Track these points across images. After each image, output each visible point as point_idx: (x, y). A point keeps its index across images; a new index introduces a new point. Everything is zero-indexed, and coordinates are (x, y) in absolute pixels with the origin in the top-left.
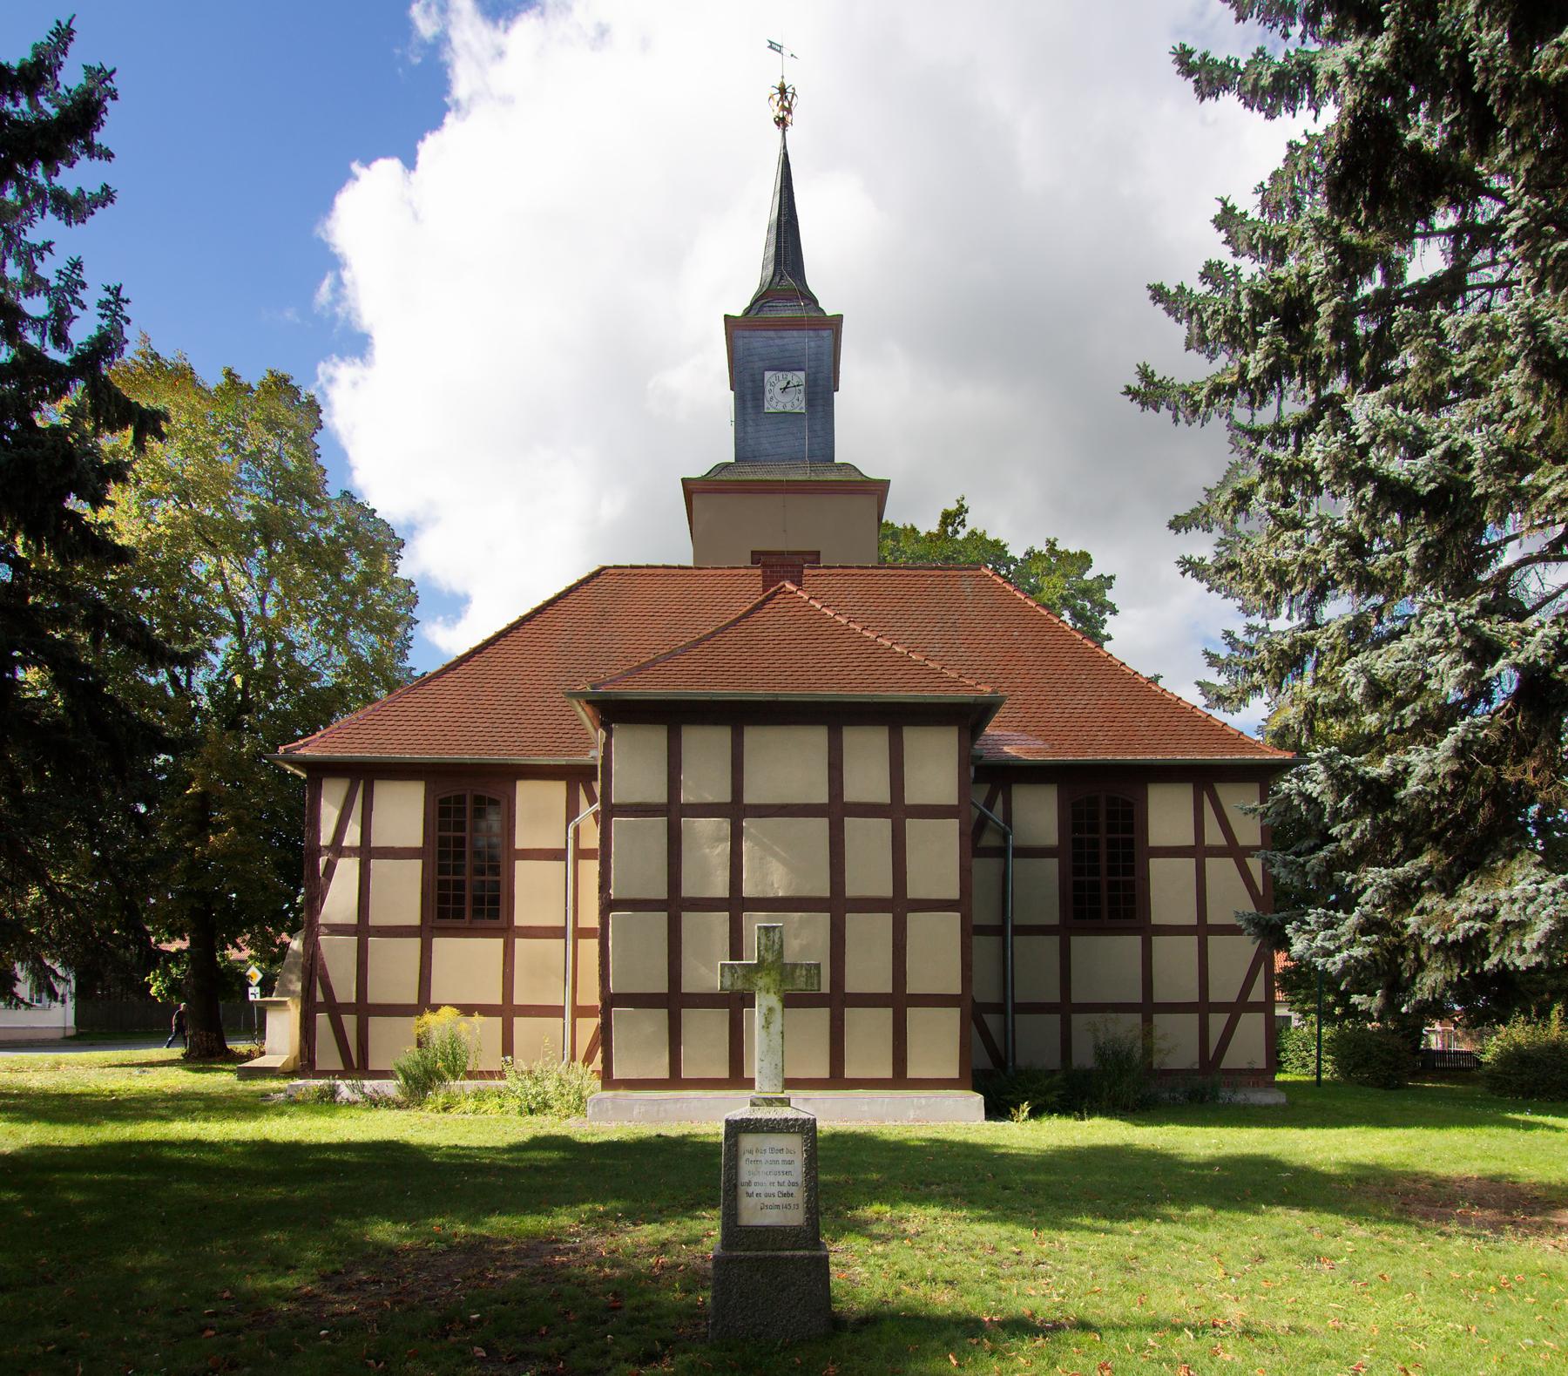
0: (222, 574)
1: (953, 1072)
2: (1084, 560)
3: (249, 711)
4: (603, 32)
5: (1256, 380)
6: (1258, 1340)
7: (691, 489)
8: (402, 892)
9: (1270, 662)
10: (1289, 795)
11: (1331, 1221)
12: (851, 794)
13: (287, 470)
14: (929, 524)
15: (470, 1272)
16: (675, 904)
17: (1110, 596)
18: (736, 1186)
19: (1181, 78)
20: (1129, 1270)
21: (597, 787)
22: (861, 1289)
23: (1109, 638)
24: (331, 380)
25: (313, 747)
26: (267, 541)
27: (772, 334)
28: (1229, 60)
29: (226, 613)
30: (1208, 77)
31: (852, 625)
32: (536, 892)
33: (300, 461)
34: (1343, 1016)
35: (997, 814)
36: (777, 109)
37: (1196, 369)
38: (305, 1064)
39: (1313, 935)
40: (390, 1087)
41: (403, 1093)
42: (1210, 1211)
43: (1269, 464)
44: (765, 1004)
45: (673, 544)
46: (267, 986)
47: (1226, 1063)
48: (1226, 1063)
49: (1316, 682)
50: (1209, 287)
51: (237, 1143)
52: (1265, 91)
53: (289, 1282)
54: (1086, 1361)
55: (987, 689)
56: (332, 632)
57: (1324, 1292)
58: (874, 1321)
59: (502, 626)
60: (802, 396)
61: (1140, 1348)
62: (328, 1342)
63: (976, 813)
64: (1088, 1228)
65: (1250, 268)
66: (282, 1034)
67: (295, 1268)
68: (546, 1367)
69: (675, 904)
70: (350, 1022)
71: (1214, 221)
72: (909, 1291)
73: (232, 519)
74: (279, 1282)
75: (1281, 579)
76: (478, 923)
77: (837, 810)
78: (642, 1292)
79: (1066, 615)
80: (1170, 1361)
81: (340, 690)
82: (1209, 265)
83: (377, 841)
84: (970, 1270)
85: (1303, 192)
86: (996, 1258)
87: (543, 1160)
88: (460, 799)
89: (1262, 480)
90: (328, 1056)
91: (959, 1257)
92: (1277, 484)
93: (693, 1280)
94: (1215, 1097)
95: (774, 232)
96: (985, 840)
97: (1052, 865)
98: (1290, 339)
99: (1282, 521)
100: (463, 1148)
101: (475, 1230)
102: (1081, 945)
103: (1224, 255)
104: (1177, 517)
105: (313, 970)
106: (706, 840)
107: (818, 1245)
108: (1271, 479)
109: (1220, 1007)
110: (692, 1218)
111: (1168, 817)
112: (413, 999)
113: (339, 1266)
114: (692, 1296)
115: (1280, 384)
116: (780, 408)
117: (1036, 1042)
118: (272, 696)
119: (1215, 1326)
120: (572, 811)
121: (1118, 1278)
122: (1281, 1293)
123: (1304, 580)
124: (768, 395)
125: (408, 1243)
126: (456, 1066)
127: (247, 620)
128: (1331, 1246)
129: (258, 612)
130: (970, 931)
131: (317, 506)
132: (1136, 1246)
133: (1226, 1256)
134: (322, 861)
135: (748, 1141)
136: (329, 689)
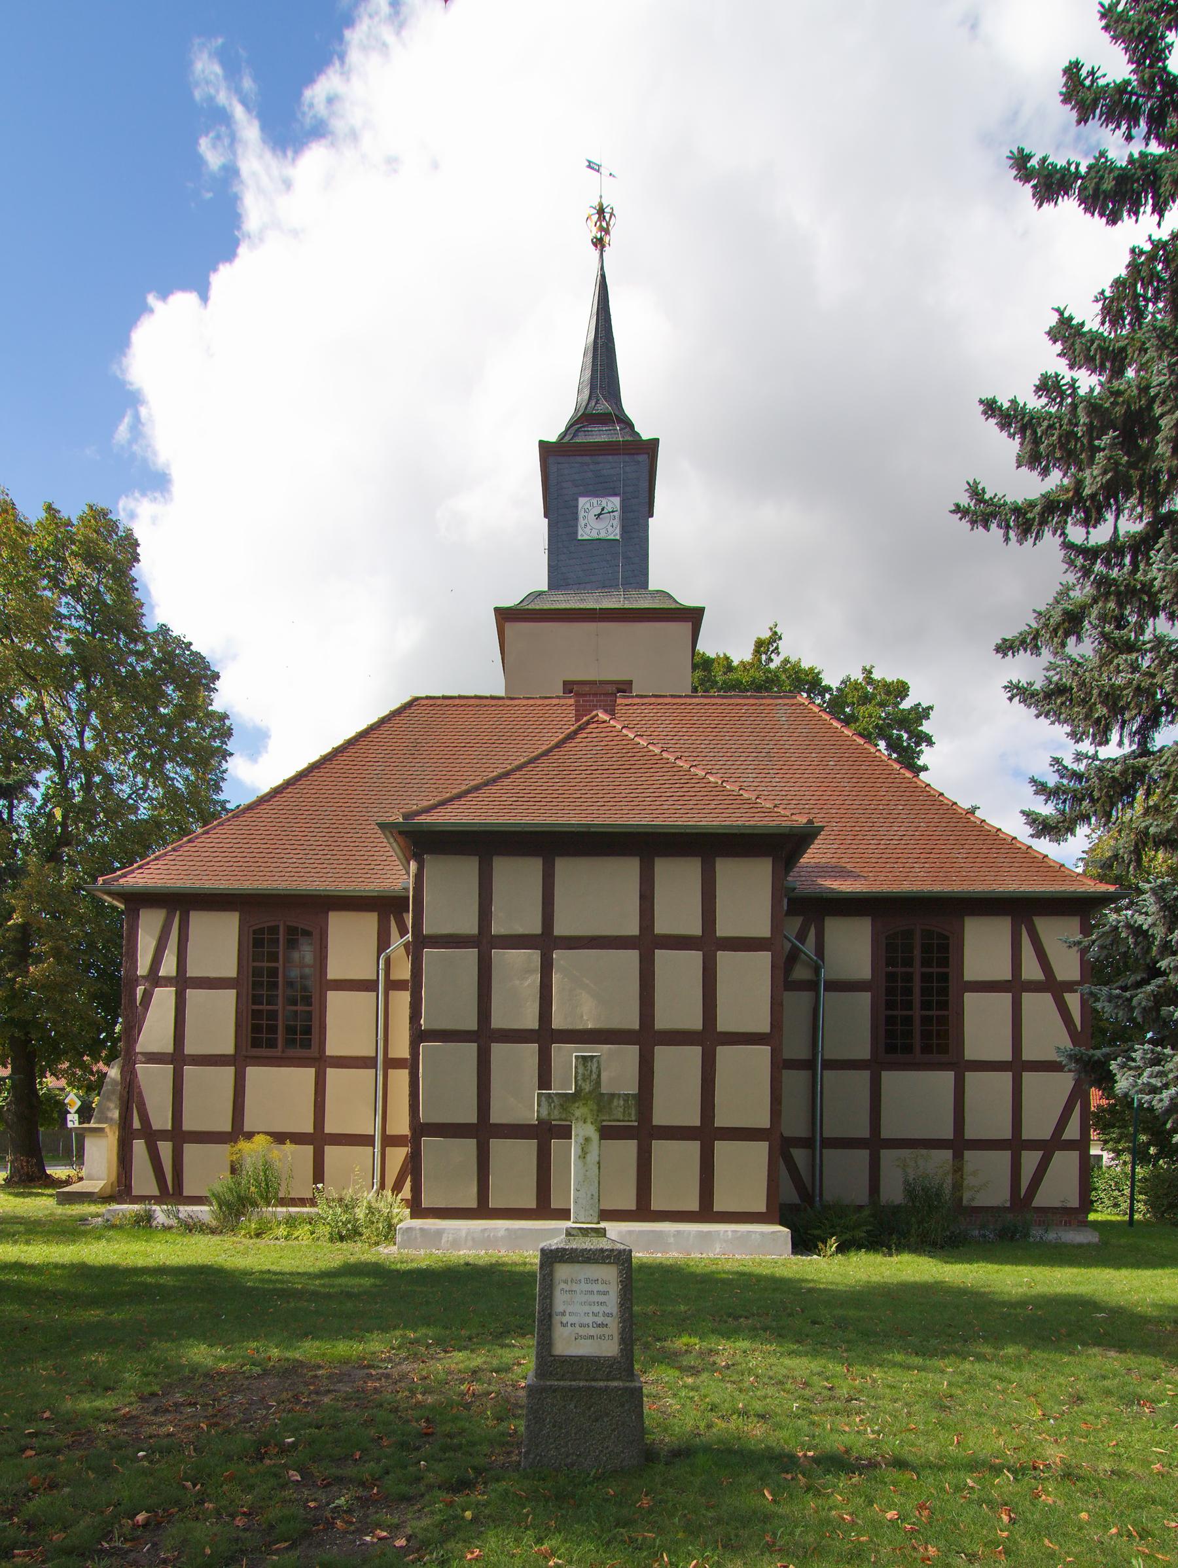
0: (43, 708)
1: (760, 1205)
2: (901, 690)
3: (68, 844)
4: (392, 162)
5: (1093, 497)
6: (1080, 1484)
7: (504, 616)
8: (216, 1020)
9: (1100, 790)
10: (1116, 928)
11: (1151, 1363)
12: (662, 926)
13: (105, 604)
14: (741, 654)
15: (284, 1396)
16: (484, 1036)
17: (926, 727)
18: (550, 1316)
19: (1019, 184)
20: (944, 1408)
21: (409, 919)
22: (671, 1420)
23: (925, 768)
24: (132, 516)
25: (140, 878)
26: (86, 675)
27: (587, 459)
28: (1069, 164)
29: (45, 745)
30: (1050, 184)
31: (665, 755)
32: (347, 1023)
33: (119, 594)
34: (1158, 1157)
35: (809, 948)
36: (594, 230)
37: (1029, 486)
38: (122, 1190)
39: (1139, 1071)
40: (203, 1212)
41: (217, 1218)
42: (1024, 1350)
43: (1103, 582)
44: (582, 1133)
45: (484, 675)
46: (85, 1113)
47: (1039, 1201)
48: (1039, 1201)
49: (1147, 811)
50: (1044, 400)
51: (56, 1266)
52: (1107, 196)
53: (105, 1403)
54: (903, 1500)
55: (802, 820)
56: (148, 765)
57: (1146, 1436)
58: (683, 1453)
59: (315, 758)
60: (616, 523)
61: (958, 1489)
62: (146, 1464)
63: (788, 946)
64: (901, 1366)
65: (1088, 382)
66: (99, 1160)
67: (112, 1389)
68: (361, 1492)
69: (484, 1036)
70: (165, 1149)
71: (1048, 333)
72: (721, 1424)
73: (51, 651)
74: (98, 1403)
75: (1115, 704)
76: (291, 1052)
77: (647, 943)
78: (455, 1419)
79: (882, 745)
80: (991, 1503)
81: (156, 823)
82: (1045, 378)
83: (192, 971)
84: (781, 1405)
85: (1147, 300)
86: (807, 1392)
87: (352, 1287)
88: (274, 930)
89: (1095, 601)
90: (144, 1180)
91: (770, 1391)
92: (1112, 605)
93: (506, 1410)
94: (1026, 1235)
95: (590, 355)
96: (796, 975)
97: (865, 998)
98: (1127, 453)
99: (1115, 645)
100: (275, 1273)
101: (288, 1354)
102: (891, 1079)
103: (1060, 367)
104: (1004, 640)
105: (130, 1096)
106: (516, 970)
107: (630, 1374)
108: (1106, 600)
109: (1033, 1145)
110: (502, 1346)
111: (985, 950)
112: (227, 1127)
113: (156, 1388)
114: (505, 1424)
115: (1117, 501)
116: (594, 535)
117: (844, 1176)
118: (91, 829)
119: (1035, 1468)
120: (383, 943)
121: (933, 1417)
122: (1102, 1435)
123: (1139, 706)
124: (582, 522)
125: (223, 1366)
126: (269, 1193)
127: (67, 753)
128: (1151, 1389)
129: (77, 745)
130: (779, 1065)
131: (134, 639)
132: (950, 1384)
133: (1044, 1396)
134: (140, 990)
135: (563, 1271)
136: (146, 821)
